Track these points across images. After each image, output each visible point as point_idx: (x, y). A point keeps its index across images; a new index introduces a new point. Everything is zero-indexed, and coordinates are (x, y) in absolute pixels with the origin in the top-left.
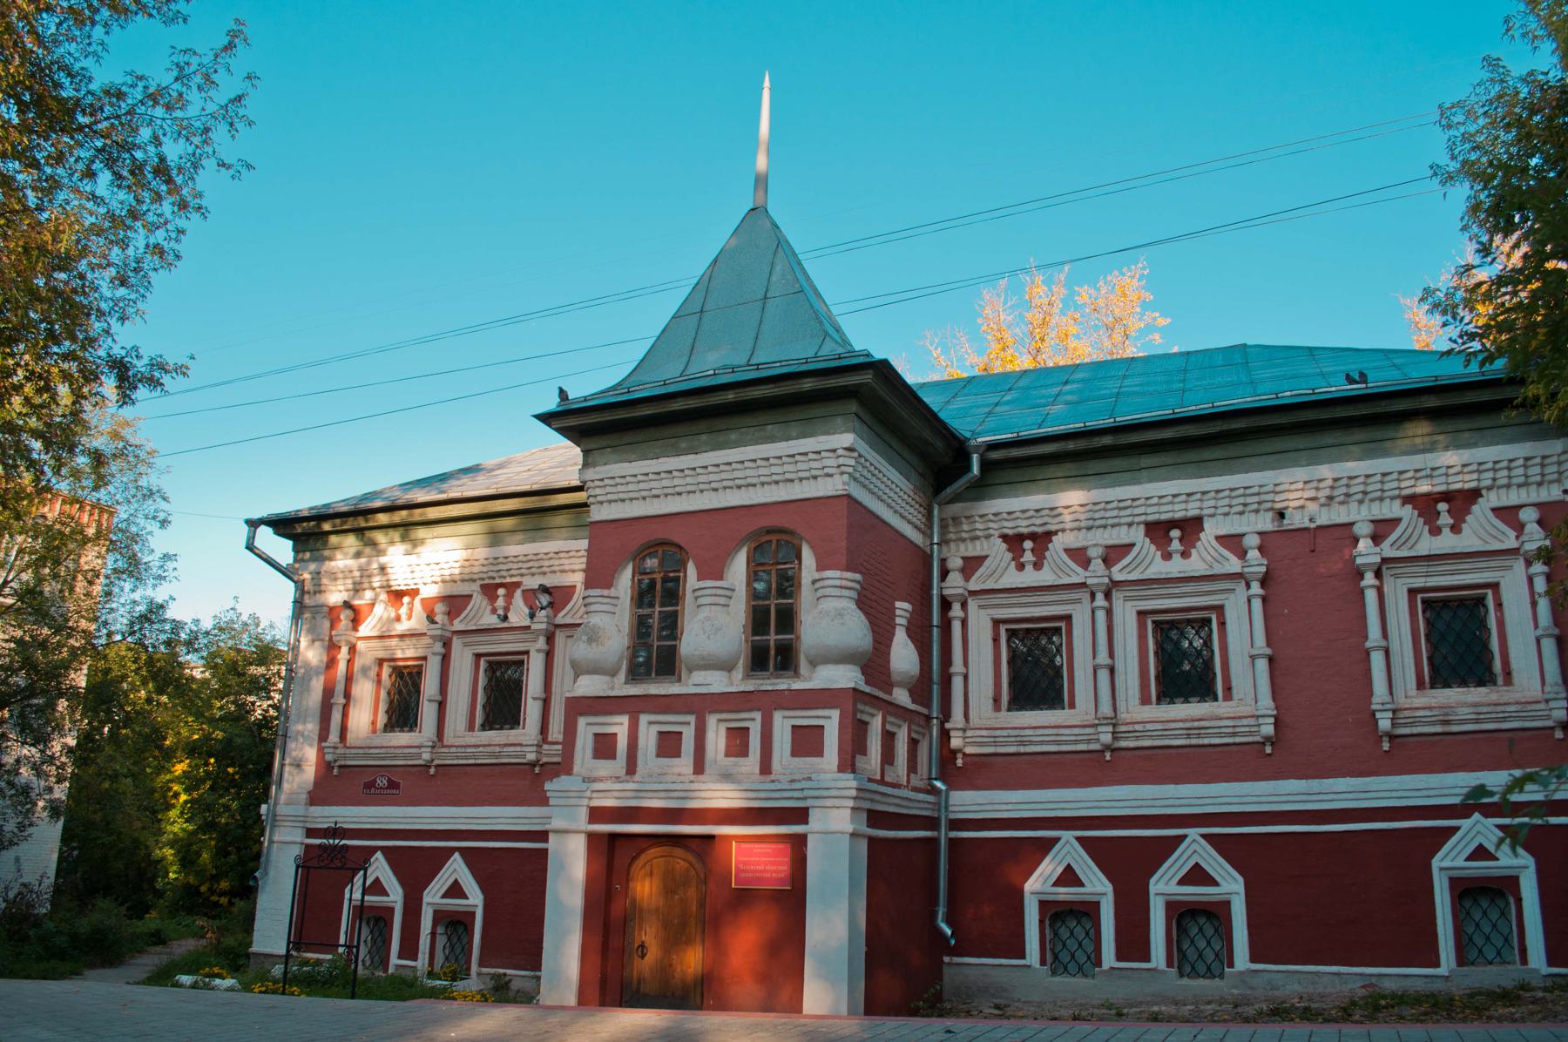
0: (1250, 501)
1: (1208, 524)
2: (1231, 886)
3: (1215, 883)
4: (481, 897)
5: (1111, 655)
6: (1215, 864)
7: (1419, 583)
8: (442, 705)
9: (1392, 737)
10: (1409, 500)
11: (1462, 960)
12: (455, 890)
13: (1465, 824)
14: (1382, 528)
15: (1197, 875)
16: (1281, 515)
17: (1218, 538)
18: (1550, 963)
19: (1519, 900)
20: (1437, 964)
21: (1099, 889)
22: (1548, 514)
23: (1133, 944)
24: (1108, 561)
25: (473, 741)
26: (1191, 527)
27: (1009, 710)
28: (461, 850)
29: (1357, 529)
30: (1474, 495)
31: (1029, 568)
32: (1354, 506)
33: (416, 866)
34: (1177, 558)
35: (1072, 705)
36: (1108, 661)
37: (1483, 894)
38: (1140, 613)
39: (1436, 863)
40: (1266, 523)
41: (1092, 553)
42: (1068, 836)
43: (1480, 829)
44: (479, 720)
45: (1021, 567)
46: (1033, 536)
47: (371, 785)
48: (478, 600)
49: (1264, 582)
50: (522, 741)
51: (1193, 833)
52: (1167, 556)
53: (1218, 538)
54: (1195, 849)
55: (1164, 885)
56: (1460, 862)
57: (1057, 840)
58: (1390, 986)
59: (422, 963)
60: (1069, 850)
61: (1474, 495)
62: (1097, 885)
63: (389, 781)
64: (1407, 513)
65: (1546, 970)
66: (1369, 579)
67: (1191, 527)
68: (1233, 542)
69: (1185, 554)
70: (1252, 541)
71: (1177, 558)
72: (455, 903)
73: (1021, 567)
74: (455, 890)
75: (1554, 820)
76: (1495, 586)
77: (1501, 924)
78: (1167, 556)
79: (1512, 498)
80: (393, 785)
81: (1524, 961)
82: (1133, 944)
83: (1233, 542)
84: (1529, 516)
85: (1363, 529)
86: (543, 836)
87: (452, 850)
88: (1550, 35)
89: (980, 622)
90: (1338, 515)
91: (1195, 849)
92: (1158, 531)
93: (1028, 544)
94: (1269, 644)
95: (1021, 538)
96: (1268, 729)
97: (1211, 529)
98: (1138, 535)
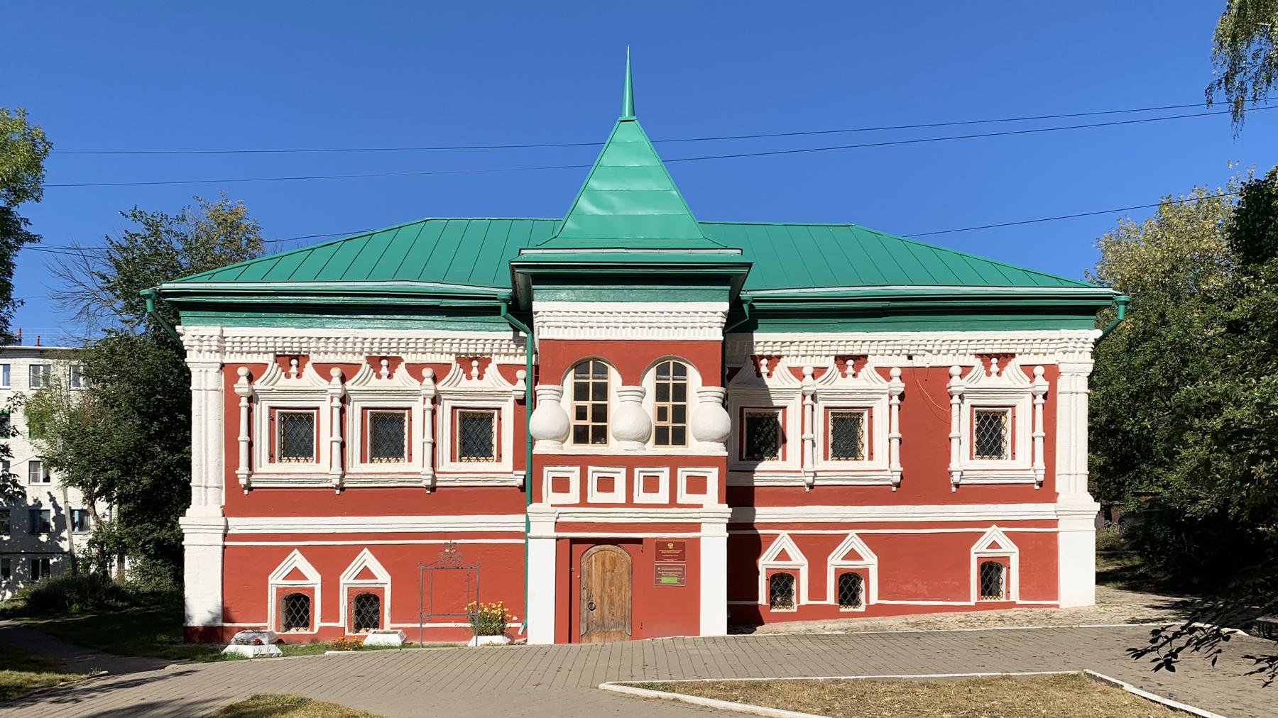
0: (893, 347)
4: (319, 577)
5: (342, 434)
8: (250, 444)
9: (957, 486)
13: (988, 530)
14: (966, 369)
15: (853, 555)
20: (338, 621)
22: (907, 374)
23: (330, 611)
26: (860, 360)
28: (299, 548)
29: (952, 371)
31: (850, 377)
32: (950, 355)
33: (331, 558)
36: (340, 439)
38: (364, 409)
39: (973, 550)
41: (805, 371)
42: (784, 533)
43: (994, 534)
45: (844, 376)
49: (1045, 397)
50: (500, 469)
51: (852, 532)
54: (784, 541)
57: (777, 535)
59: (342, 622)
60: (994, 534)
64: (978, 363)
66: (956, 399)
68: (884, 372)
70: (896, 372)
73: (844, 376)
74: (783, 555)
78: (288, 376)
81: (1008, 597)
82: (330, 611)
83: (884, 372)
84: (1039, 371)
85: (955, 371)
86: (696, 527)
87: (362, 547)
89: (262, 412)
91: (853, 541)
93: (994, 360)
95: (990, 356)
96: (898, 479)
97: (873, 362)
98: (830, 362)
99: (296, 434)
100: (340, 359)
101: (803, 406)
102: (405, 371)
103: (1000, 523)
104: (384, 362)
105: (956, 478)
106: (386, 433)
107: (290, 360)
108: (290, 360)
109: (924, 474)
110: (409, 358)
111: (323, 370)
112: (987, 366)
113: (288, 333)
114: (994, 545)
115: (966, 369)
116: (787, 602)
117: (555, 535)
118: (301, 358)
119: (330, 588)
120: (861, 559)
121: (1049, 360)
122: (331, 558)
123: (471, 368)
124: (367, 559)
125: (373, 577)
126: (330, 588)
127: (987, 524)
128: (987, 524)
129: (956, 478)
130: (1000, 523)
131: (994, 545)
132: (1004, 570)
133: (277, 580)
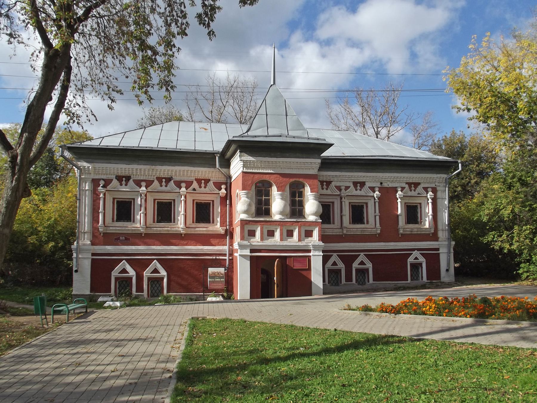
1: (367, 183)
2: (369, 265)
3: (365, 265)
6: (366, 261)
7: (407, 201)
10: (407, 183)
11: (411, 280)
12: (335, 264)
13: (414, 252)
14: (347, 188)
16: (381, 183)
17: (369, 187)
18: (427, 280)
19: (422, 268)
21: (342, 266)
23: (349, 278)
24: (346, 190)
25: (350, 227)
26: (363, 184)
27: (117, 221)
30: (419, 184)
31: (325, 189)
33: (140, 264)
34: (358, 190)
35: (334, 223)
37: (416, 267)
40: (379, 185)
42: (335, 254)
43: (416, 254)
44: (115, 219)
45: (323, 189)
46: (326, 182)
47: (118, 239)
48: (156, 183)
51: (362, 254)
52: (356, 190)
53: (369, 187)
54: (362, 257)
55: (355, 265)
56: (117, 274)
58: (399, 285)
59: (145, 293)
60: (416, 254)
61: (419, 184)
62: (341, 265)
63: (125, 238)
64: (407, 186)
65: (426, 281)
67: (363, 184)
69: (360, 190)
71: (358, 190)
72: (335, 267)
73: (356, 190)
75: (217, 257)
76: (420, 204)
77: (152, 289)
79: (426, 186)
80: (126, 239)
81: (422, 280)
88: (283, 45)
90: (394, 185)
91: (362, 257)
92: (355, 184)
94: (379, 212)
99: (124, 211)
100: (104, 177)
101: (375, 203)
102: (212, 184)
103: (419, 250)
104: (164, 180)
105: (401, 231)
106: (165, 211)
107: (123, 179)
108: (123, 179)
109: (389, 230)
110: (177, 178)
111: (138, 183)
112: (410, 187)
113: (123, 168)
114: (416, 258)
115: (347, 188)
116: (364, 283)
117: (249, 254)
118: (128, 178)
119: (140, 278)
120: (365, 265)
121: (433, 186)
122: (140, 264)
123: (357, 186)
124: (156, 264)
125: (127, 273)
126: (140, 278)
127: (413, 250)
128: (413, 250)
129: (401, 231)
130: (419, 250)
131: (416, 258)
132: (420, 268)
133: (115, 273)
